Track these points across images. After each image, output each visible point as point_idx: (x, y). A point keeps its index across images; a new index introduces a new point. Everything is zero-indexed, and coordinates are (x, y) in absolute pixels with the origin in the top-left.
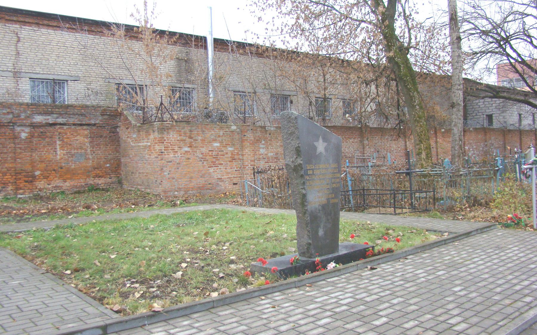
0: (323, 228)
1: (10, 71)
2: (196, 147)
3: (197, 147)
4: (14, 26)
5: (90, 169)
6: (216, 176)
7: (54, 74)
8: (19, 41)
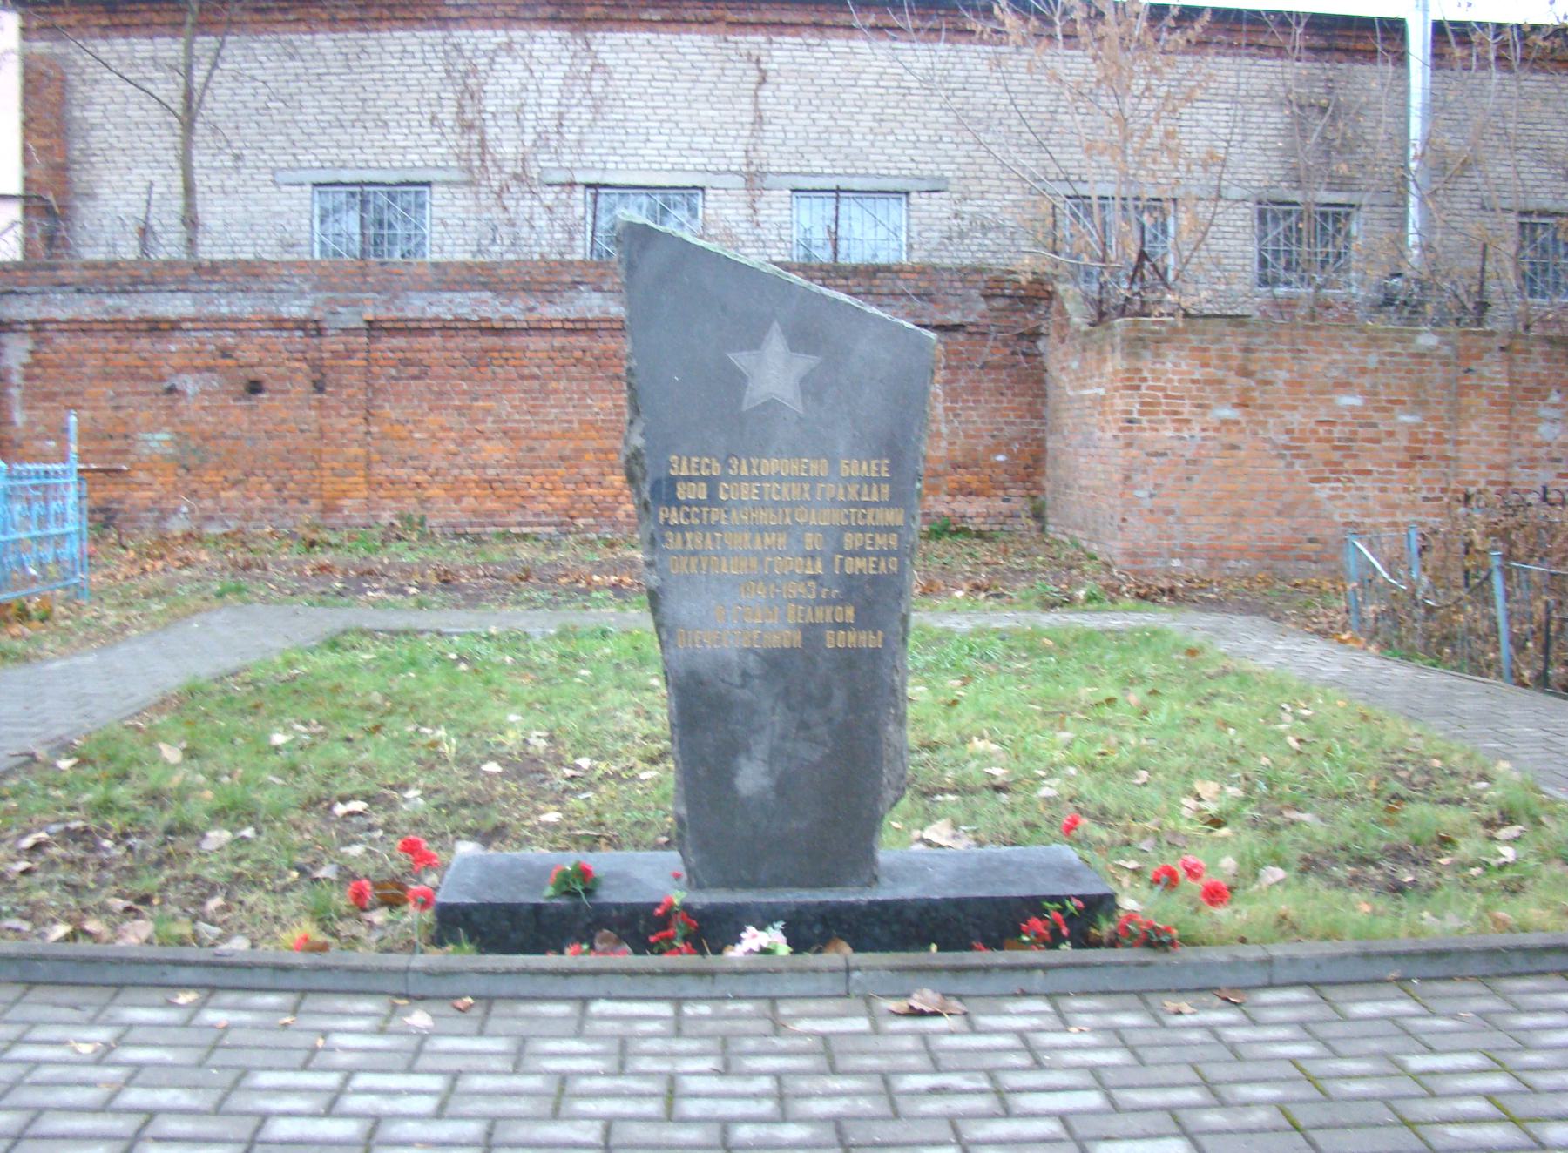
0: (770, 761)
1: (735, 173)
2: (1263, 407)
3: (1270, 407)
4: (750, 38)
5: (940, 468)
6: (1337, 514)
7: (867, 175)
8: (763, 80)
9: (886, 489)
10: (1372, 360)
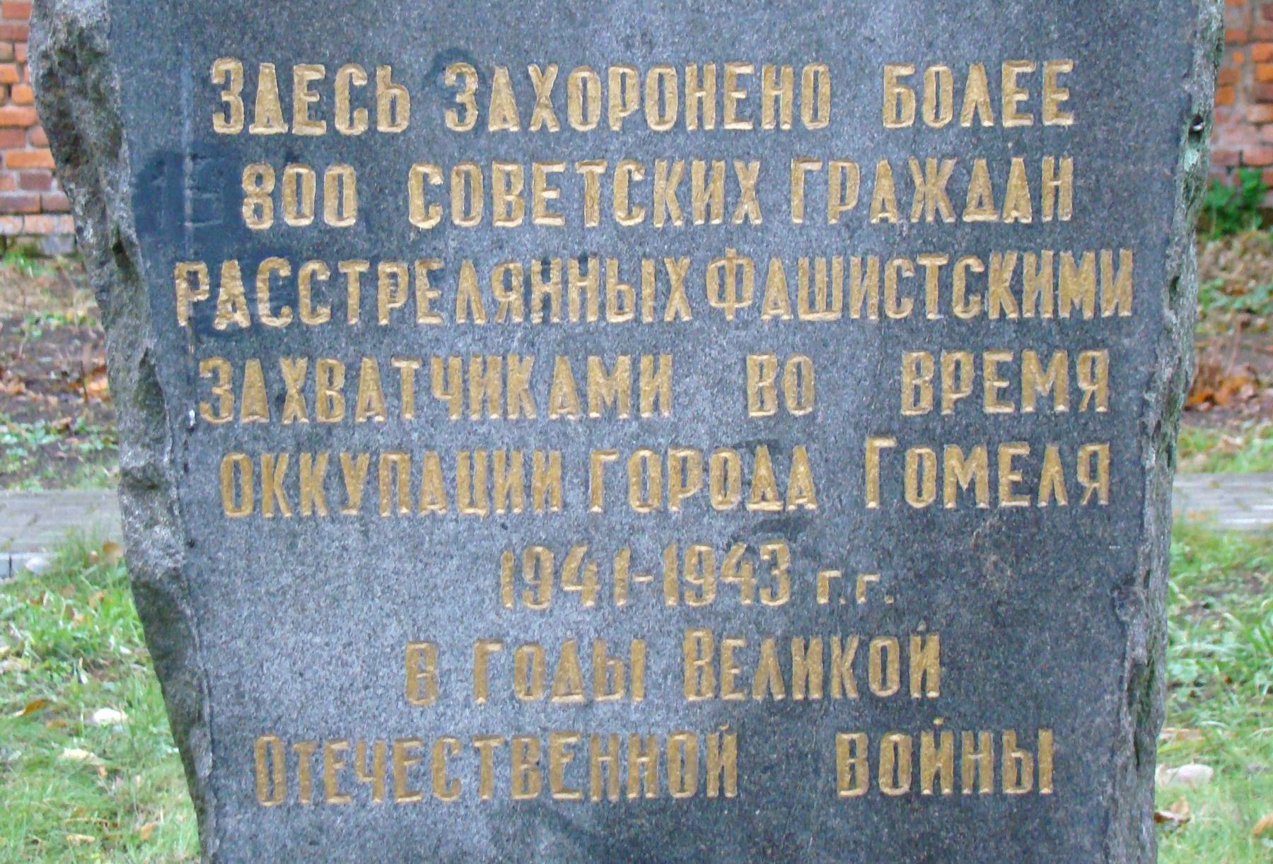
9: (1061, 176)
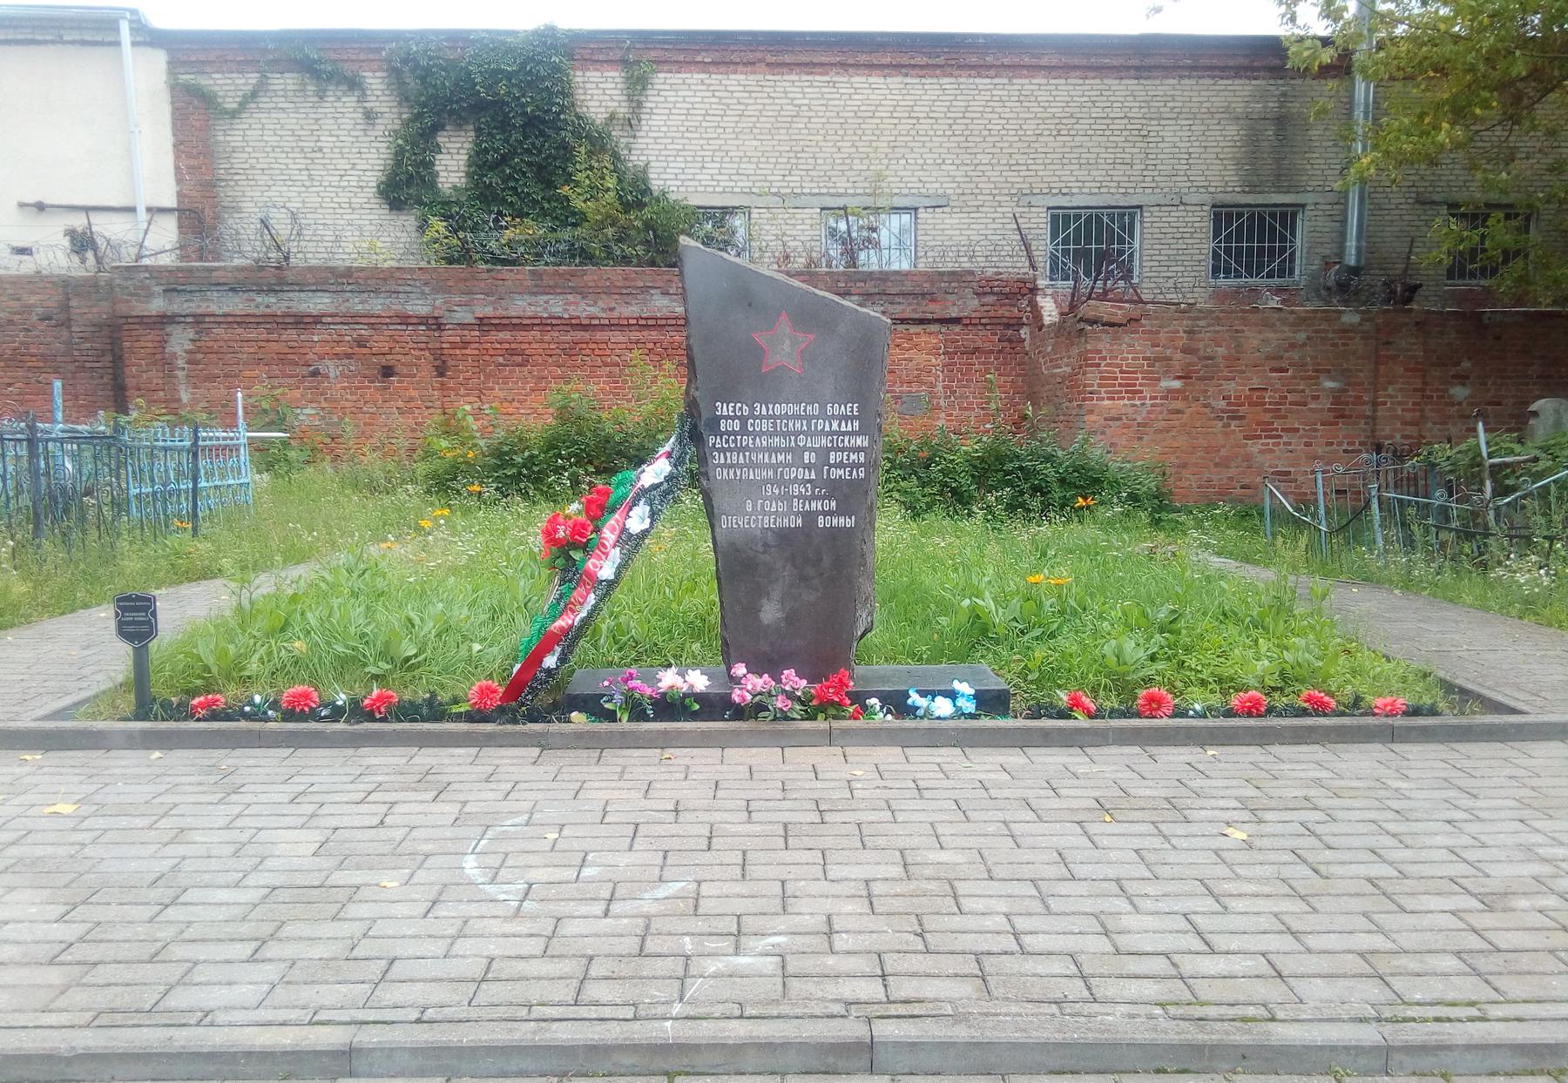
0: (782, 601)
9: (856, 424)
10: (1301, 337)
